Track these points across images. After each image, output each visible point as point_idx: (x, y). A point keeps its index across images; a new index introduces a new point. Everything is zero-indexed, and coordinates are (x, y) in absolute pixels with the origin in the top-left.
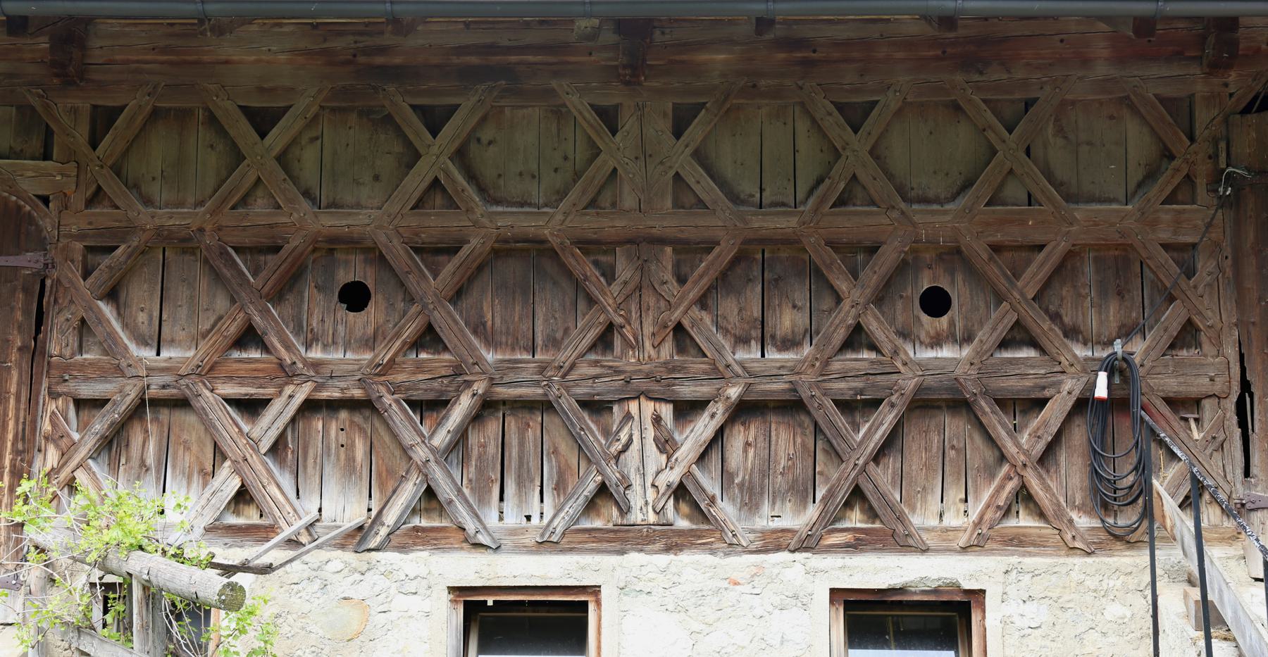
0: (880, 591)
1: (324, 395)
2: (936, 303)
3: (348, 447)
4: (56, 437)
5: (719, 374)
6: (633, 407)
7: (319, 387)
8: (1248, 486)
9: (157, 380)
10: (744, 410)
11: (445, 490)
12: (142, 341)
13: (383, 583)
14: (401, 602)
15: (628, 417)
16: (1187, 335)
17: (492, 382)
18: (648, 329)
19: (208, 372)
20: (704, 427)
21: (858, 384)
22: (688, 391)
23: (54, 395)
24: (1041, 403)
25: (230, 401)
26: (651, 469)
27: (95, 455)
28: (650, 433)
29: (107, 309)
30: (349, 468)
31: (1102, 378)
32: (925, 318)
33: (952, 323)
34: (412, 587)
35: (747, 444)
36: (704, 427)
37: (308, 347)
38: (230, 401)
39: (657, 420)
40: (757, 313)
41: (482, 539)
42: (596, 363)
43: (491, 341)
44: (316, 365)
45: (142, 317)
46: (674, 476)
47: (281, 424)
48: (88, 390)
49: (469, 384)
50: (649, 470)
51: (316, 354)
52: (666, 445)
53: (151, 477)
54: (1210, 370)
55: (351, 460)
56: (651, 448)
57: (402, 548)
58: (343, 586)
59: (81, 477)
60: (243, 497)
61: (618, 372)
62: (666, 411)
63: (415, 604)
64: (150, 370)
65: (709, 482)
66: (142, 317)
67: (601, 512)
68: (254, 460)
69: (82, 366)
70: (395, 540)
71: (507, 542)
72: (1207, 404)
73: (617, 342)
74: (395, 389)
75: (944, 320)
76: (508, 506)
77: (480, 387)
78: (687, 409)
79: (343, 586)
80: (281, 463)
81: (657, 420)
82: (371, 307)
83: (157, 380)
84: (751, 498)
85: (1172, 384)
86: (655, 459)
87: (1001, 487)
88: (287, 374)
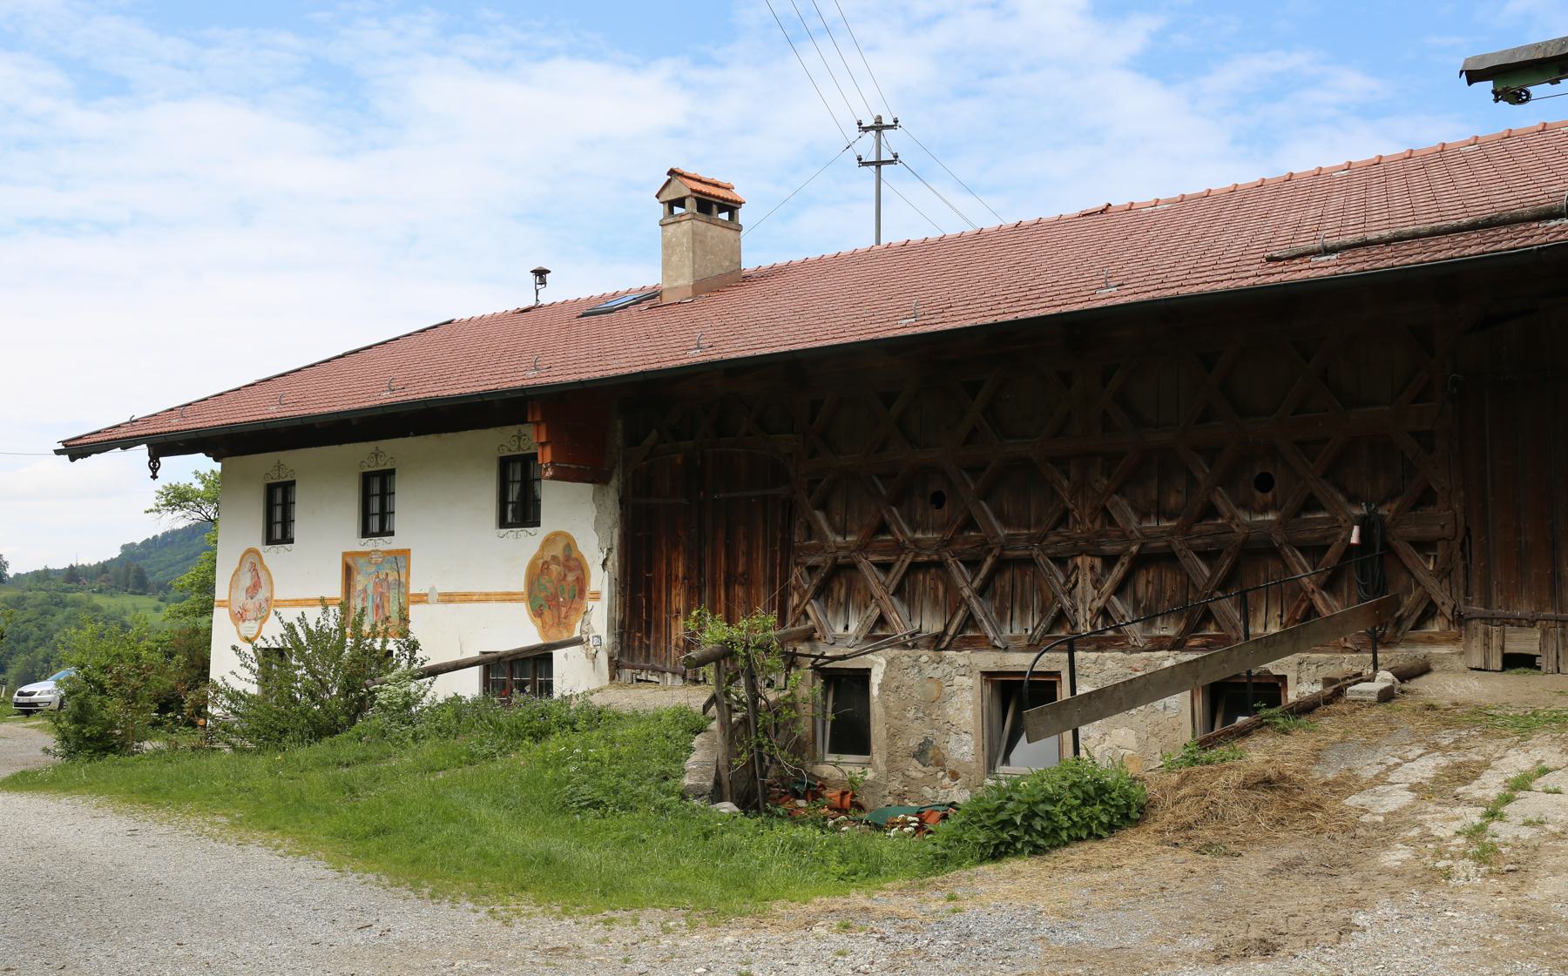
0: (105, 431)
1: (920, 559)
2: (1265, 483)
3: (936, 589)
4: (797, 588)
5: (1126, 537)
6: (1079, 560)
7: (917, 555)
8: (1467, 603)
9: (841, 554)
10: (1141, 561)
11: (979, 615)
12: (838, 532)
13: (948, 669)
14: (958, 680)
15: (1076, 567)
16: (1426, 498)
17: (1003, 548)
18: (1088, 511)
19: (863, 548)
20: (1118, 572)
21: (1208, 540)
22: (1108, 549)
23: (797, 564)
24: (1327, 547)
25: (874, 564)
26: (1089, 599)
27: (816, 596)
28: (1089, 577)
29: (820, 515)
30: (935, 602)
31: (1356, 530)
32: (1258, 494)
33: (1274, 496)
34: (962, 671)
35: (1148, 582)
36: (1118, 572)
37: (915, 531)
38: (874, 564)
39: (1092, 568)
40: (1154, 497)
41: (997, 643)
42: (1059, 534)
43: (1006, 523)
44: (915, 542)
45: (837, 518)
46: (1099, 603)
47: (899, 577)
48: (811, 561)
49: (991, 550)
50: (1086, 600)
51: (919, 535)
52: (1097, 584)
53: (842, 609)
54: (1440, 521)
55: (936, 597)
56: (1089, 586)
57: (958, 649)
58: (929, 671)
59: (808, 608)
60: (882, 621)
61: (1069, 538)
62: (1098, 562)
63: (967, 682)
64: (839, 548)
65: (1121, 607)
66: (837, 518)
67: (1059, 631)
68: (886, 597)
69: (807, 548)
70: (954, 644)
71: (1011, 644)
72: (1439, 544)
73: (1071, 520)
74: (955, 554)
75: (1270, 494)
76: (1016, 624)
77: (996, 552)
78: (1110, 561)
79: (929, 671)
80: (902, 599)
81: (1092, 568)
82: (946, 507)
83: (841, 554)
84: (1149, 618)
85: (1414, 531)
86: (1091, 592)
87: (1299, 607)
88: (899, 548)
